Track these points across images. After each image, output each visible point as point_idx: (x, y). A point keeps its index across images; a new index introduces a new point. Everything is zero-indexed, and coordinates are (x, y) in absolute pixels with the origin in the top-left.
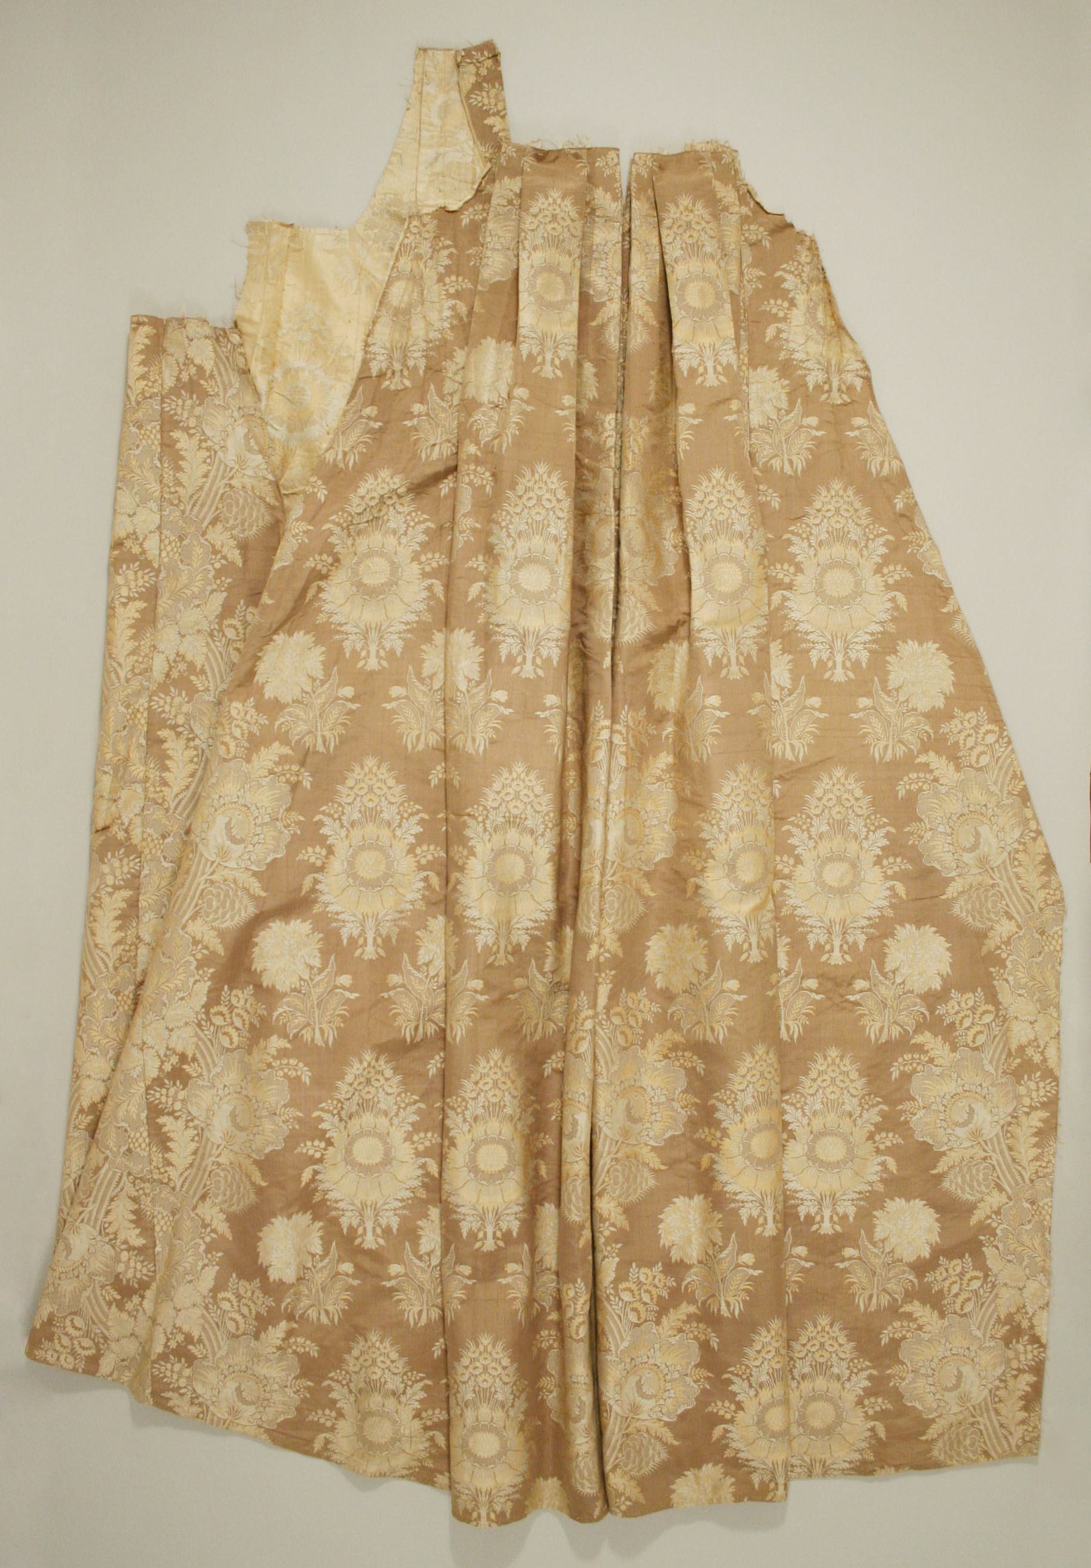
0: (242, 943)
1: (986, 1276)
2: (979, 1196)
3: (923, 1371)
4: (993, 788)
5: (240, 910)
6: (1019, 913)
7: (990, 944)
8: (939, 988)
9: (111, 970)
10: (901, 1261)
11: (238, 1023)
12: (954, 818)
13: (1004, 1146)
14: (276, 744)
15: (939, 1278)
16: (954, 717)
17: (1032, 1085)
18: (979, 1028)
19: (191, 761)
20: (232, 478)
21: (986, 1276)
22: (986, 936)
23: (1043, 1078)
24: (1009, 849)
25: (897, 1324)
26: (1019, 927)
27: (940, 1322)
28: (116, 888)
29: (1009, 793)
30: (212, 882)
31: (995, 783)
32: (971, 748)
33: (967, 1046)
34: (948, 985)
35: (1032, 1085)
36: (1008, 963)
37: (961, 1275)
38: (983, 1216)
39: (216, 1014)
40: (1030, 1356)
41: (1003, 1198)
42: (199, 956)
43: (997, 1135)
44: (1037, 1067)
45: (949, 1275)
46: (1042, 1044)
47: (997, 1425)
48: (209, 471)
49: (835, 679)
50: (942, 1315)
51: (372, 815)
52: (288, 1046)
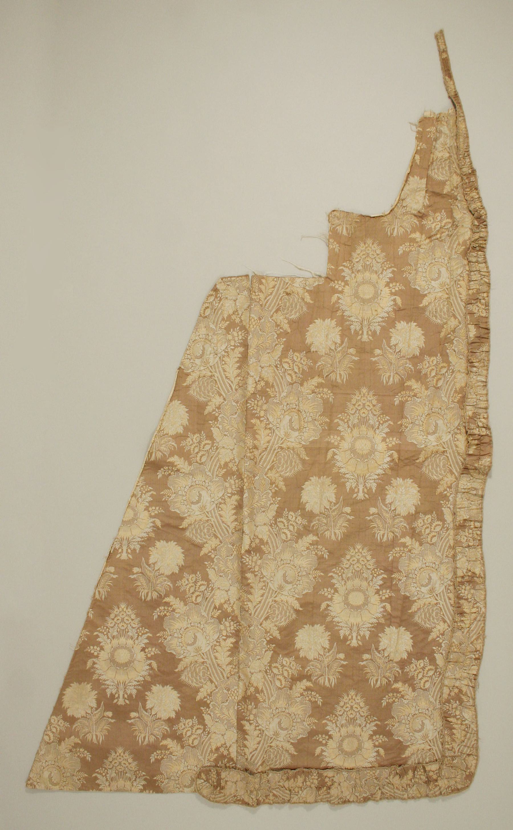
0: (289, 632)
3: (180, 493)
5: (284, 760)
8: (174, 717)
9: (230, 533)
11: (296, 370)
12: (417, 570)
14: (305, 681)
15: (189, 444)
18: (434, 534)
19: (258, 736)
20: (287, 288)
24: (216, 502)
27: (185, 608)
28: (233, 494)
30: (275, 601)
31: (210, 471)
38: (202, 697)
39: (280, 522)
42: (278, 332)
48: (276, 285)
49: (119, 703)
51: (358, 574)
52: (323, 381)
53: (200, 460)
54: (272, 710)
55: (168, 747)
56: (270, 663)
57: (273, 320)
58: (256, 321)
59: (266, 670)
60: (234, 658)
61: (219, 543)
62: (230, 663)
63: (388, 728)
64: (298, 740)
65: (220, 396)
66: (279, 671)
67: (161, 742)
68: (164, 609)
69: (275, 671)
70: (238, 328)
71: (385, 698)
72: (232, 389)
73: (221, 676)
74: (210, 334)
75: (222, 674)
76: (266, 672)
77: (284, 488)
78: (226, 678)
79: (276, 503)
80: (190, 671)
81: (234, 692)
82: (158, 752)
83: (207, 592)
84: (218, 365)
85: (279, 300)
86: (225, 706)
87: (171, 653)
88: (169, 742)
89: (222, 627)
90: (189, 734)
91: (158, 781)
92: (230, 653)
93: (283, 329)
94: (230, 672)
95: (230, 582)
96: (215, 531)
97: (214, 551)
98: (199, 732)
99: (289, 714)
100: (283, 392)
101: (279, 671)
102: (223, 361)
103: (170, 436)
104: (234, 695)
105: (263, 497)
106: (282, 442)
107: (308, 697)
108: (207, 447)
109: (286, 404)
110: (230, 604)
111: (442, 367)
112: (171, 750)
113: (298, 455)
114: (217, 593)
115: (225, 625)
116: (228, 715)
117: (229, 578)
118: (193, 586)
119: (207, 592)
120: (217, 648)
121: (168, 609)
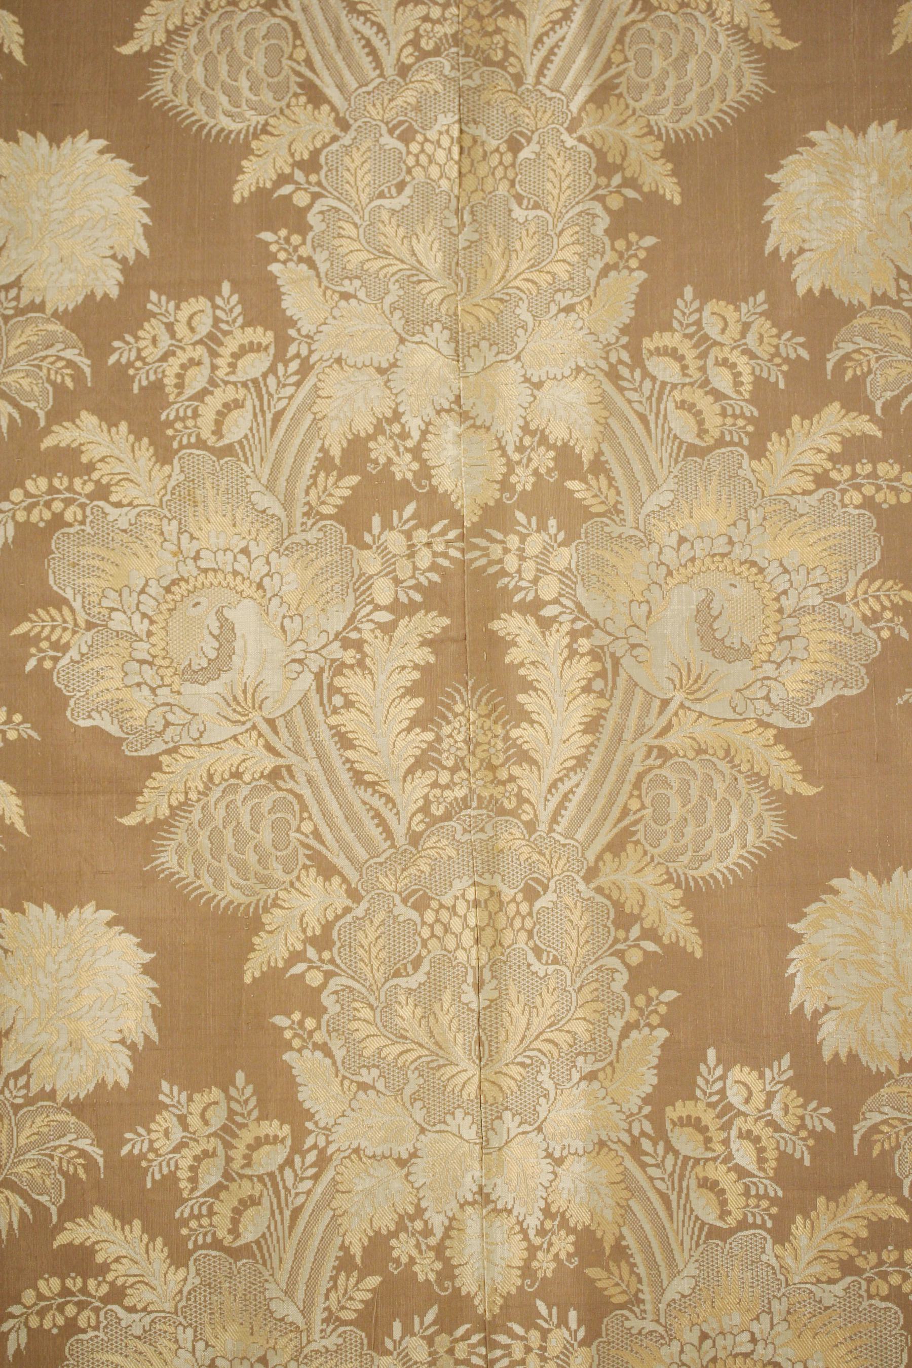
1: (283, 341)
3: (118, 621)
6: (351, 859)
7: (268, 951)
8: (125, 1082)
10: (52, 1095)
13: (325, 735)
15: (152, 353)
17: (395, 541)
18: (230, 394)
19: (587, 689)
21: (283, 341)
22: (256, 925)
24: (315, 661)
25: (38, 485)
26: (354, 895)
27: (160, 473)
32: (200, 396)
33: (201, 444)
34: (137, 276)
35: (395, 541)
37: (212, 342)
38: (280, 955)
43: (303, 702)
44: (405, 492)
45: (176, 337)
47: (345, 777)
50: (164, 454)
53: (218, 432)
54: (676, 1346)
55: (100, 1258)
56: (657, 1101)
57: (581, 139)
58: (495, 160)
59: (635, 1141)
62: (421, 763)
63: (32, 664)
64: (817, 711)
65: (327, 878)
66: (684, 368)
67: (47, 431)
68: (52, 490)
69: (665, 370)
71: (16, 1309)
73: (376, 833)
74: (254, 550)
76: (613, 375)
77: (672, 192)
79: (655, 1020)
81: (453, 910)
82: (29, 484)
83: (281, 385)
85: (627, 787)
87: (95, 729)
88: (87, 433)
89: (370, 562)
90: (197, 380)
91: (38, 639)
92: (419, 702)
93: (638, 188)
94: (415, 43)
95: (399, 325)
96: (316, 834)
98: (254, 366)
99: (754, 564)
100: (672, 1277)
101: (684, 368)
102: (338, 691)
103: (66, 1104)
105: (566, 238)
106: (663, 721)
107: (884, 1276)
108: (269, 1159)
109: (693, 1337)
111: (243, 351)
112: (101, 473)
113: (758, 779)
114: (334, 383)
115: (383, 550)
116: (425, 1040)
117: (408, 1091)
119: (281, 385)
121: (70, 489)
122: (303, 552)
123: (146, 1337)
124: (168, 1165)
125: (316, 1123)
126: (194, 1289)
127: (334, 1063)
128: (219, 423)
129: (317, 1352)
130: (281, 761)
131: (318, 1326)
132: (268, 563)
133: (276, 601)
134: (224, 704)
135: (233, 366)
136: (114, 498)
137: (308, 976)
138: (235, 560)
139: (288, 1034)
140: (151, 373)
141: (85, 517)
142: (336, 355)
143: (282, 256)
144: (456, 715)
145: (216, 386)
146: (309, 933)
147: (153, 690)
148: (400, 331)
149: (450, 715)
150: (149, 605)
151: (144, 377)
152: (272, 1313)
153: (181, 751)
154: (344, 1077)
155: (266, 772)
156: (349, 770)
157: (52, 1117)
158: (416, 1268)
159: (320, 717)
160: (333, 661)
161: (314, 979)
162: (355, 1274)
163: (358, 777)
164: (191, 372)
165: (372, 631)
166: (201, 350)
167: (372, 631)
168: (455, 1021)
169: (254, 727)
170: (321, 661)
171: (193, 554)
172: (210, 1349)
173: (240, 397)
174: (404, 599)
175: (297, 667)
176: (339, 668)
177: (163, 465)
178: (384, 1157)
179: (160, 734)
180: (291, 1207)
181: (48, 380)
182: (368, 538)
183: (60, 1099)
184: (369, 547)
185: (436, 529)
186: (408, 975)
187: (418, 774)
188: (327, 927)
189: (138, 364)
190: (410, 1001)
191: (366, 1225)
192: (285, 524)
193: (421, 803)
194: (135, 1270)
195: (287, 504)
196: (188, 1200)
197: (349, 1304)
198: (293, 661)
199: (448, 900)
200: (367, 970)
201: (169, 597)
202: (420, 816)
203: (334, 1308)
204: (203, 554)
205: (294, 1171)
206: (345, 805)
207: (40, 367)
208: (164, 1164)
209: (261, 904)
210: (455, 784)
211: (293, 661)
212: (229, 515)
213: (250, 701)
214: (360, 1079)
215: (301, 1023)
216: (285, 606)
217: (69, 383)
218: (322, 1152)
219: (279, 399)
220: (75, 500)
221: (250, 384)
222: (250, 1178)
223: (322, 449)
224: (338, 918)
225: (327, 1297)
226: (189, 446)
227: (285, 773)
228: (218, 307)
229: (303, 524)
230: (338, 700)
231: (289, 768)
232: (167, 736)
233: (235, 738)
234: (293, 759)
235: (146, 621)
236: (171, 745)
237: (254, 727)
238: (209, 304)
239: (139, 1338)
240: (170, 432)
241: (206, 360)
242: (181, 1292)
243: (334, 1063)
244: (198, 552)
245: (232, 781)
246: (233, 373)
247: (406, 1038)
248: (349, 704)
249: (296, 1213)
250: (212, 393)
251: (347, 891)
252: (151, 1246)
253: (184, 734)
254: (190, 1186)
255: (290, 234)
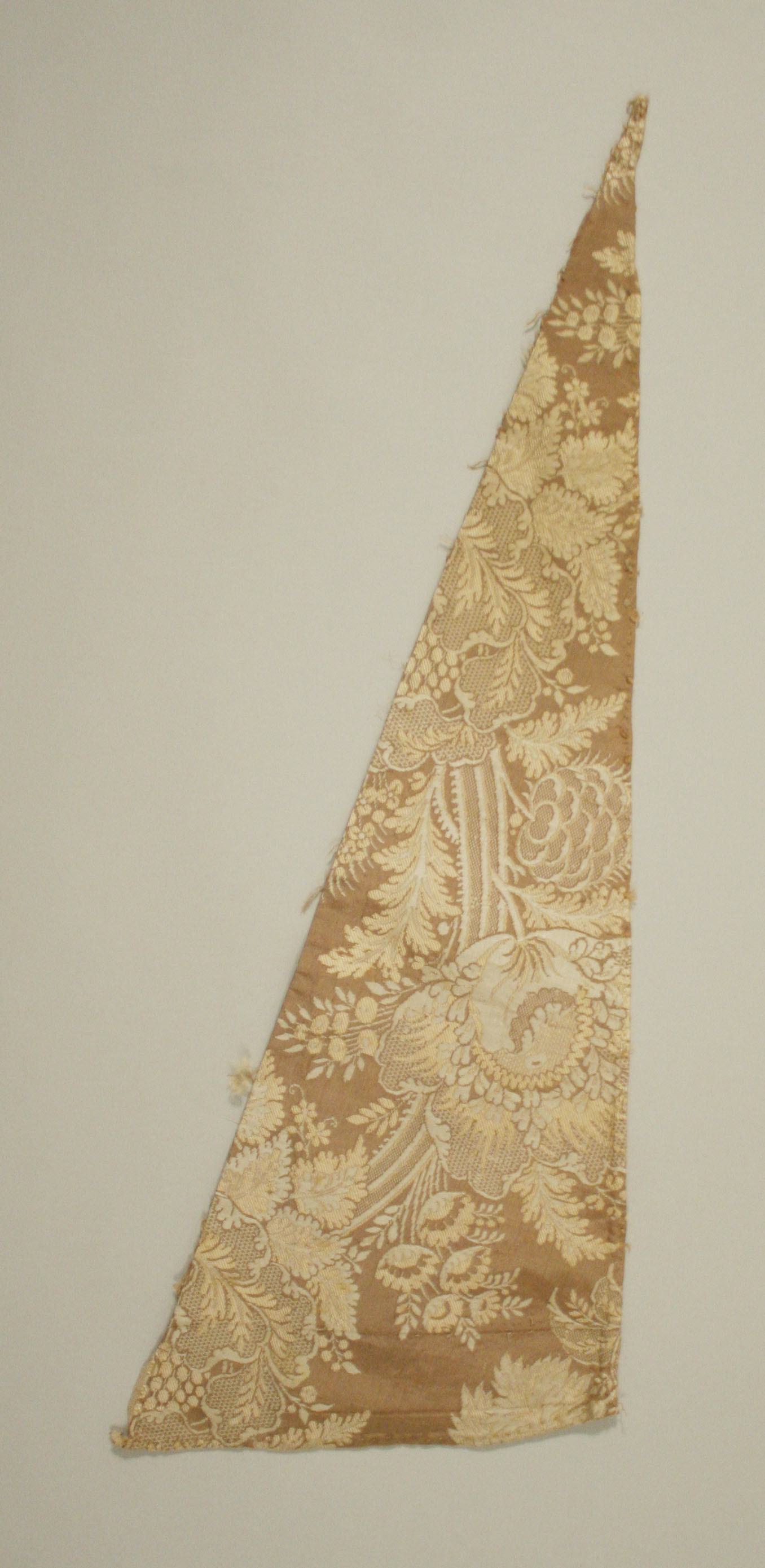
2: (578, 769)
4: (442, 1133)
6: (490, 771)
12: (568, 1089)
15: (491, 1297)
16: (483, 1330)
17: (338, 1051)
18: (436, 1237)
21: (371, 1265)
23: (306, 1060)
26: (502, 735)
27: (523, 1187)
29: (402, 1106)
31: (430, 1140)
32: (462, 1244)
33: (478, 1200)
36: (305, 1370)
37: (434, 1288)
38: (589, 706)
40: (321, 1024)
41: (520, 743)
43: (474, 940)
46: (283, 1142)
47: (464, 855)
50: (514, 1202)
53: (458, 1205)
55: (585, 1222)
60: (361, 856)
61: (512, 733)
62: (394, 838)
65: (519, 761)
70: (315, 1073)
72: (448, 781)
73: (459, 790)
75: (449, 796)
78: (440, 770)
80: (606, 859)
84: (475, 925)
86: (233, 1347)
89: (369, 1044)
90: (459, 1262)
92: (374, 895)
95: (263, 1239)
96: (511, 809)
97: (297, 1415)
98: (405, 1255)
102: (440, 938)
104: (173, 1385)
110: (294, 1138)
114: (338, 1212)
117: (263, 1262)
118: (450, 1277)
119: (386, 1228)
120: (425, 942)
122: (424, 1075)
123: (567, 1149)
124: (493, 1281)
125: (352, 1269)
126: (511, 1172)
127: (318, 1314)
128: (455, 1212)
129: (425, 1084)
130: (518, 891)
131: (415, 1104)
132: (458, 1077)
133: (464, 1040)
134: (545, 963)
135: (422, 1261)
136: (571, 1182)
137: (313, 1399)
138: (486, 1091)
139: (607, 636)
140: (497, 1282)
141: (605, 1176)
142: (327, 1235)
143: (603, 626)
144: (346, 867)
145: (443, 1249)
146: (555, 716)
147: (603, 998)
148: (263, 1232)
149: (352, 870)
150: (579, 1077)
151: (506, 1280)
152: (451, 1132)
153: (600, 932)
154: (315, 1297)
155: (533, 886)
156: (459, 860)
157: (581, 1349)
158: (314, 1114)
159: (466, 918)
160: (435, 966)
161: (565, 676)
162: (368, 1131)
163: (453, 850)
164: (462, 1269)
165: (390, 978)
166: (445, 1285)
167: (390, 978)
168: (203, 1306)
169: (528, 931)
170: (445, 969)
171: (522, 1110)
172: (516, 1120)
173: (426, 1230)
174: (352, 997)
175: (468, 973)
176: (433, 958)
177: (519, 1193)
178: (306, 1216)
179: (612, 955)
180: (402, 1206)
181: (591, 1303)
182: (361, 1064)
183: (568, 1361)
184: (364, 1056)
185: (298, 1048)
186: (485, 645)
187: (399, 831)
188: (537, 716)
189: (505, 1292)
190: (234, 1339)
191: (344, 1165)
192: (430, 1103)
193: (409, 801)
194: (557, 1205)
195: (421, 1119)
196: (488, 1246)
197: (383, 1111)
198: (470, 980)
199: (425, 695)
200: (517, 665)
201: (558, 1078)
202: (416, 787)
203: (396, 1114)
204: (513, 1107)
205: (386, 1236)
206: (474, 829)
207: (594, 1318)
208: (497, 1282)
209: (586, 759)
210: (372, 804)
211: (470, 980)
212: (475, 1131)
213: (521, 960)
214: (301, 1289)
215: (592, 641)
216: (459, 1032)
217: (573, 1296)
218: (357, 1241)
219: (392, 1215)
220: (608, 1193)
221: (413, 1239)
222: (426, 1245)
223: (371, 1156)
224: (524, 721)
225: (399, 1124)
226: (489, 1202)
227: (516, 879)
228: (416, 1316)
229: (414, 1099)
230: (444, 929)
231: (511, 882)
232: (606, 952)
233: (549, 928)
234: (506, 890)
235: (585, 1064)
236: (607, 942)
237: (528, 931)
238: (424, 1323)
239: (575, 1151)
240: (501, 1220)
241: (444, 1275)
242: (523, 1174)
243: (318, 1314)
244: (517, 1110)
245: (564, 890)
246: (423, 1256)
247: (250, 1308)
248: (435, 921)
249: (398, 1201)
250: (450, 1243)
251: (507, 742)
252: (535, 1217)
253: (590, 949)
254: (481, 1257)
255: (587, 646)
